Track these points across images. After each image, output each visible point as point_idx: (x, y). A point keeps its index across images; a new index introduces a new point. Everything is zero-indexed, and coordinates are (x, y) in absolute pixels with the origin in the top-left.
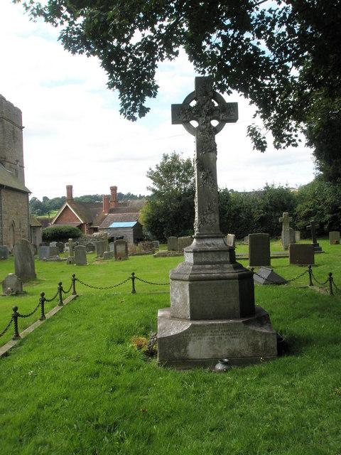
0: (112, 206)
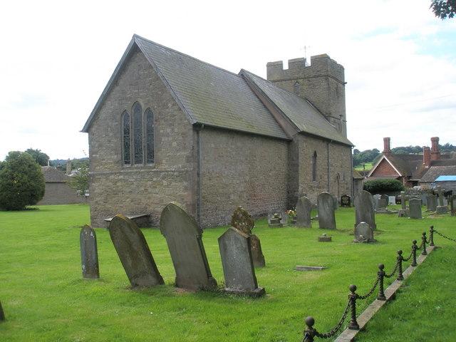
0: (434, 158)
